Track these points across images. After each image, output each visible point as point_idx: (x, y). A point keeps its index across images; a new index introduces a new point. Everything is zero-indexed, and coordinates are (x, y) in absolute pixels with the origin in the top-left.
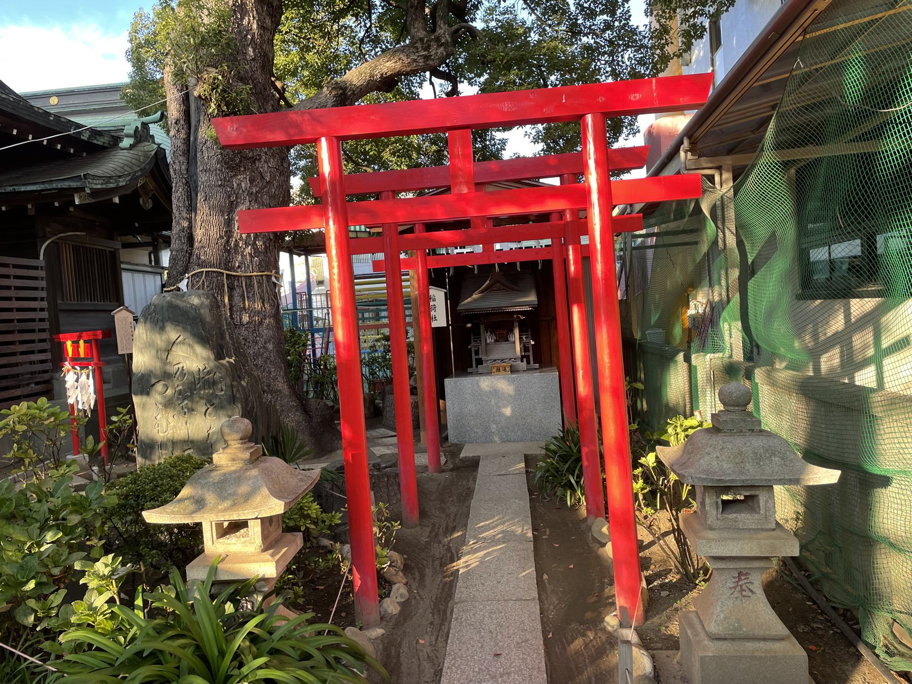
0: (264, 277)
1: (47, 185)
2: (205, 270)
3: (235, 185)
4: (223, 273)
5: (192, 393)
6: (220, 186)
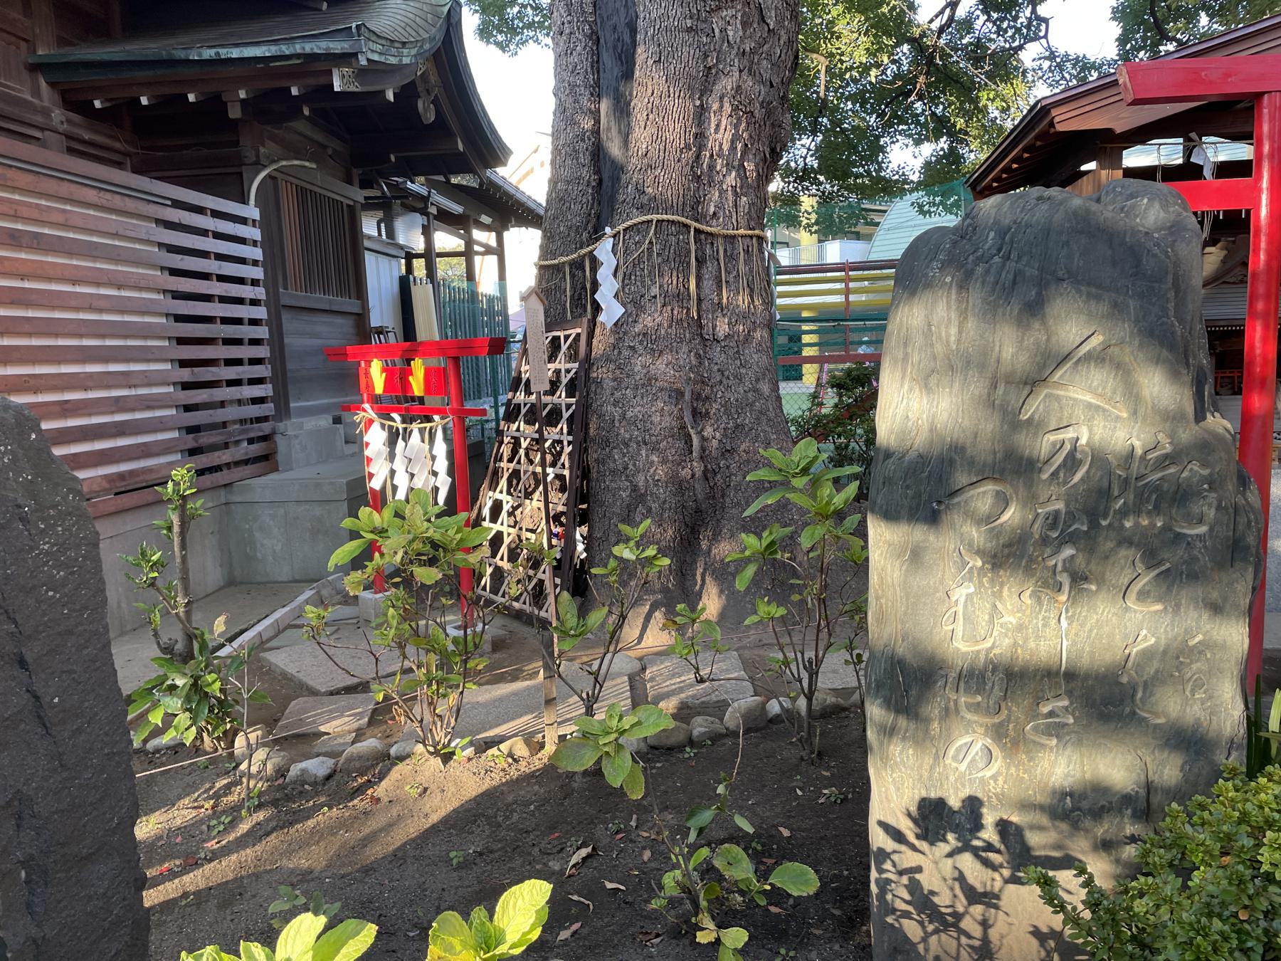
0: (754, 239)
1: (284, 48)
2: (655, 217)
3: (717, 31)
4: (687, 227)
5: (1094, 524)
6: (689, 30)
